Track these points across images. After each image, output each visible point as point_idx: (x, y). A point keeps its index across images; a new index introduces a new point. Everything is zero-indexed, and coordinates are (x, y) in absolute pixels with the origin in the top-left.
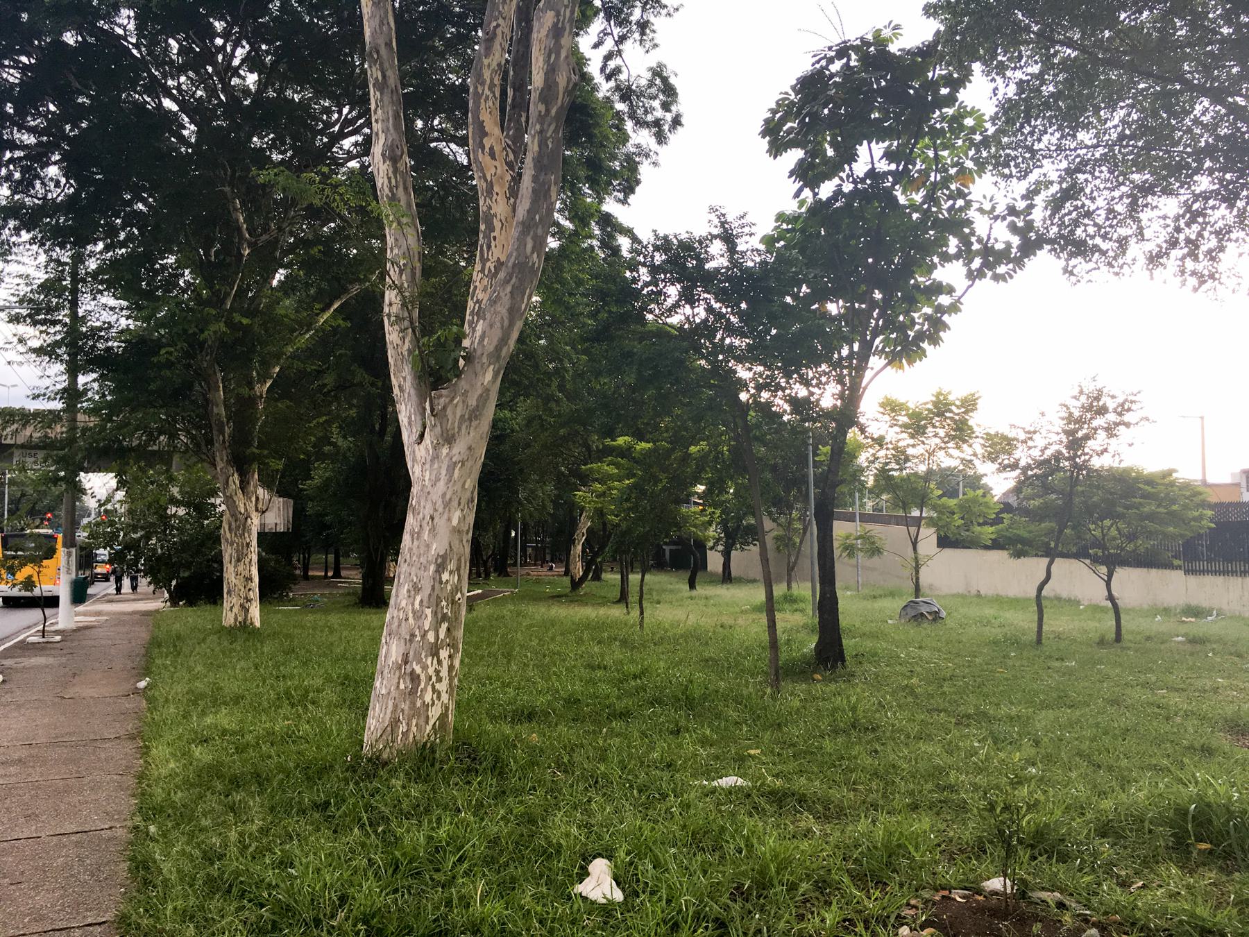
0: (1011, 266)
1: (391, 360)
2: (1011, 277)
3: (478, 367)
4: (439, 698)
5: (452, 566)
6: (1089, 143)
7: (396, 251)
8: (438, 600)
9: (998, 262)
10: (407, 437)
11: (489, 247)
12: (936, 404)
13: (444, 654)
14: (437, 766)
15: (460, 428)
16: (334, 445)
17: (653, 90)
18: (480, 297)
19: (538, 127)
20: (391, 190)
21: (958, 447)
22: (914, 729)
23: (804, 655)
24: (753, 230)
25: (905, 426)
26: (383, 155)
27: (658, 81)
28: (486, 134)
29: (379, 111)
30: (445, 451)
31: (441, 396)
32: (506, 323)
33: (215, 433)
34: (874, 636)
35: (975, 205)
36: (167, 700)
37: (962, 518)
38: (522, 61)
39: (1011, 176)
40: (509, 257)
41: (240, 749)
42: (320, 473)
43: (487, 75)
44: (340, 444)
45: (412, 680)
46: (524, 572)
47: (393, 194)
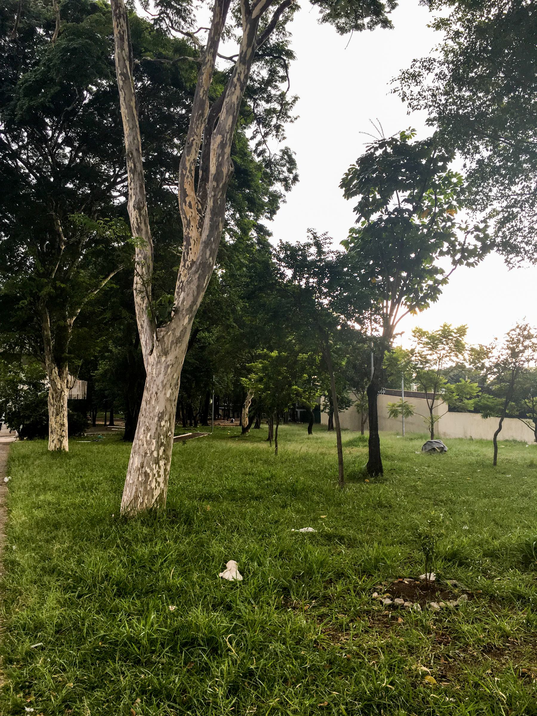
0: (476, 258)
1: (137, 312)
2: (477, 264)
3: (181, 316)
4: (159, 485)
5: (166, 418)
6: (519, 192)
7: (140, 256)
8: (159, 435)
9: (470, 256)
10: (145, 351)
11: (188, 254)
12: (444, 331)
13: (162, 463)
14: (157, 519)
15: (171, 347)
16: (111, 351)
17: (283, 162)
18: (183, 279)
19: (213, 193)
20: (138, 224)
21: (456, 356)
22: (410, 506)
23: (361, 469)
24: (332, 241)
25: (427, 343)
26: (134, 207)
27: (286, 157)
28: (187, 195)
29: (132, 184)
30: (163, 359)
31: (161, 331)
32: (195, 293)
33: (45, 345)
34: (403, 460)
35: (457, 225)
36: (19, 488)
37: (458, 395)
38: (206, 157)
39: (476, 209)
40: (197, 259)
41: (58, 511)
42: (103, 367)
43: (188, 165)
44: (114, 350)
45: (145, 476)
46: (216, 423)
47: (139, 227)
